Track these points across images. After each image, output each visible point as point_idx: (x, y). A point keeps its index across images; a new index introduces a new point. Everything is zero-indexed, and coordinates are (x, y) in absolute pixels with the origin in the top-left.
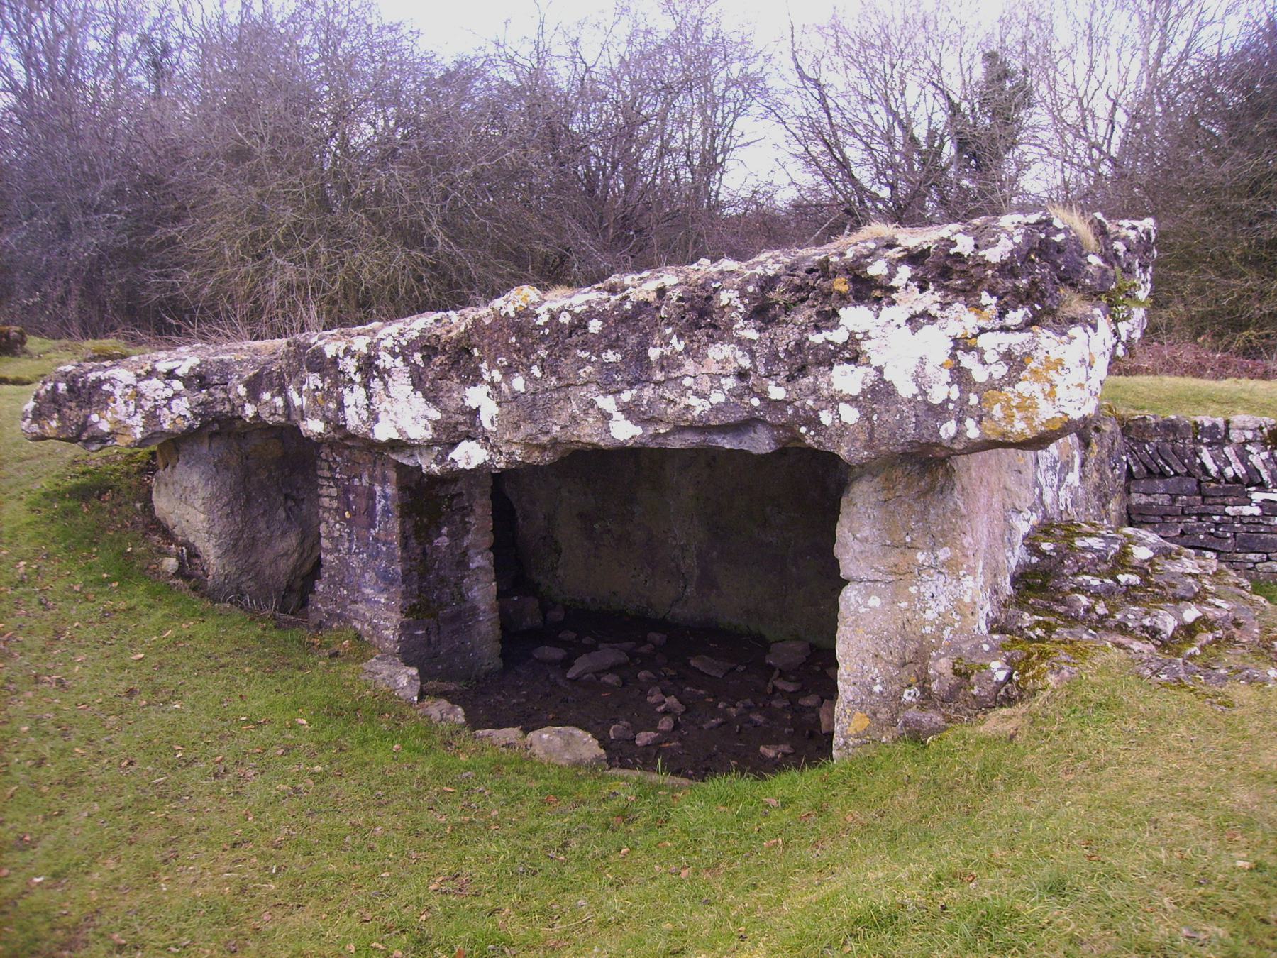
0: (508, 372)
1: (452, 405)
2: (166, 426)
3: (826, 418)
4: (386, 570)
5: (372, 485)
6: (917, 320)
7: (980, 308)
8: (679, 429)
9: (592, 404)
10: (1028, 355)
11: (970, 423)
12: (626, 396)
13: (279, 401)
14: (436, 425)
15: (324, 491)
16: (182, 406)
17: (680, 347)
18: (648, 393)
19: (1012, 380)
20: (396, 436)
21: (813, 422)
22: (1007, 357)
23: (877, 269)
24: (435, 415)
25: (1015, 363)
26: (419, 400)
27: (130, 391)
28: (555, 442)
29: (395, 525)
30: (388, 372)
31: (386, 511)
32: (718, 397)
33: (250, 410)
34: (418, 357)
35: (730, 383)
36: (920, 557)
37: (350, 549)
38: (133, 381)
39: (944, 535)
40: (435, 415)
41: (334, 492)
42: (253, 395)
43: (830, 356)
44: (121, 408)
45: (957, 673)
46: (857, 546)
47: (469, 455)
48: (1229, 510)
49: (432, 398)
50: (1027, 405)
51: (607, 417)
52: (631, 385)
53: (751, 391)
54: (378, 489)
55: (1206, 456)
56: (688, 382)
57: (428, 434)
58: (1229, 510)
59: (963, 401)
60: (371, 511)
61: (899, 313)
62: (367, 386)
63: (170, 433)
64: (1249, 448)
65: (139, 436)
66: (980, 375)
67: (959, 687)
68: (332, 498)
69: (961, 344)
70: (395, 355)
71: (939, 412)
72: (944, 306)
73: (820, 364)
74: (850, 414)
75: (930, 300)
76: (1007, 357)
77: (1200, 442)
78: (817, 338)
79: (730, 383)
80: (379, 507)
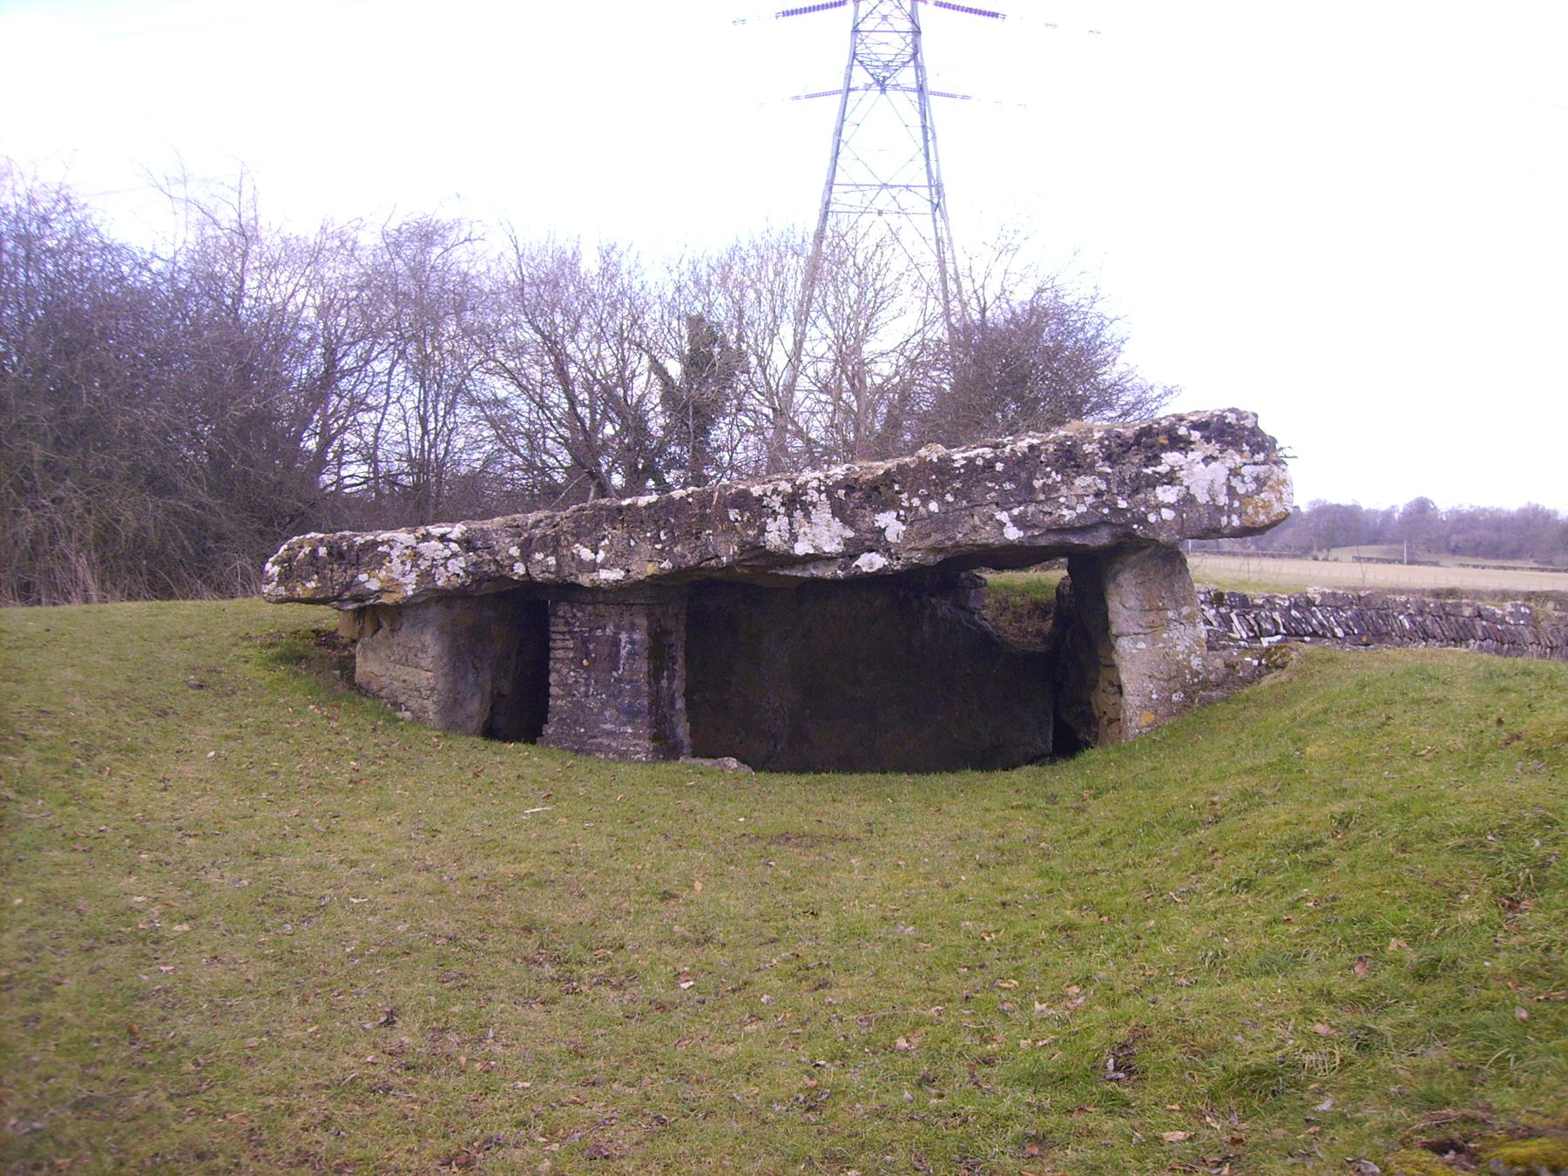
0: (925, 500)
1: (864, 526)
2: (440, 583)
3: (1152, 518)
4: (631, 705)
5: (616, 634)
6: (1207, 460)
7: (1241, 452)
8: (1049, 531)
9: (992, 517)
10: (1268, 478)
11: (1234, 517)
12: (1015, 512)
13: (552, 560)
15: (559, 644)
16: (457, 565)
17: (1059, 478)
18: (1031, 509)
19: (1258, 491)
20: (812, 551)
21: (1143, 520)
22: (1257, 479)
23: (1182, 431)
24: (850, 534)
25: (1260, 482)
26: (837, 524)
27: (408, 552)
28: (957, 545)
30: (814, 505)
31: (631, 654)
32: (1081, 509)
33: (520, 569)
34: (841, 493)
35: (1090, 500)
36: (1170, 614)
37: (586, 693)
38: (413, 542)
39: (1184, 598)
40: (850, 534)
41: (571, 644)
42: (526, 557)
45: (1227, 666)
46: (1126, 613)
47: (871, 562)
49: (848, 522)
50: (1267, 506)
51: (1002, 525)
52: (1020, 504)
53: (1104, 504)
54: (624, 637)
56: (1062, 500)
57: (840, 549)
59: (1231, 505)
60: (614, 658)
61: (1196, 455)
62: (790, 516)
63: (442, 590)
65: (410, 593)
66: (1241, 490)
67: (1228, 675)
68: (566, 649)
69: (1234, 472)
70: (820, 492)
71: (1220, 510)
72: (1221, 452)
73: (1148, 486)
74: (1167, 514)
75: (1213, 448)
76: (1257, 479)
78: (1149, 471)
79: (1090, 500)
80: (623, 652)
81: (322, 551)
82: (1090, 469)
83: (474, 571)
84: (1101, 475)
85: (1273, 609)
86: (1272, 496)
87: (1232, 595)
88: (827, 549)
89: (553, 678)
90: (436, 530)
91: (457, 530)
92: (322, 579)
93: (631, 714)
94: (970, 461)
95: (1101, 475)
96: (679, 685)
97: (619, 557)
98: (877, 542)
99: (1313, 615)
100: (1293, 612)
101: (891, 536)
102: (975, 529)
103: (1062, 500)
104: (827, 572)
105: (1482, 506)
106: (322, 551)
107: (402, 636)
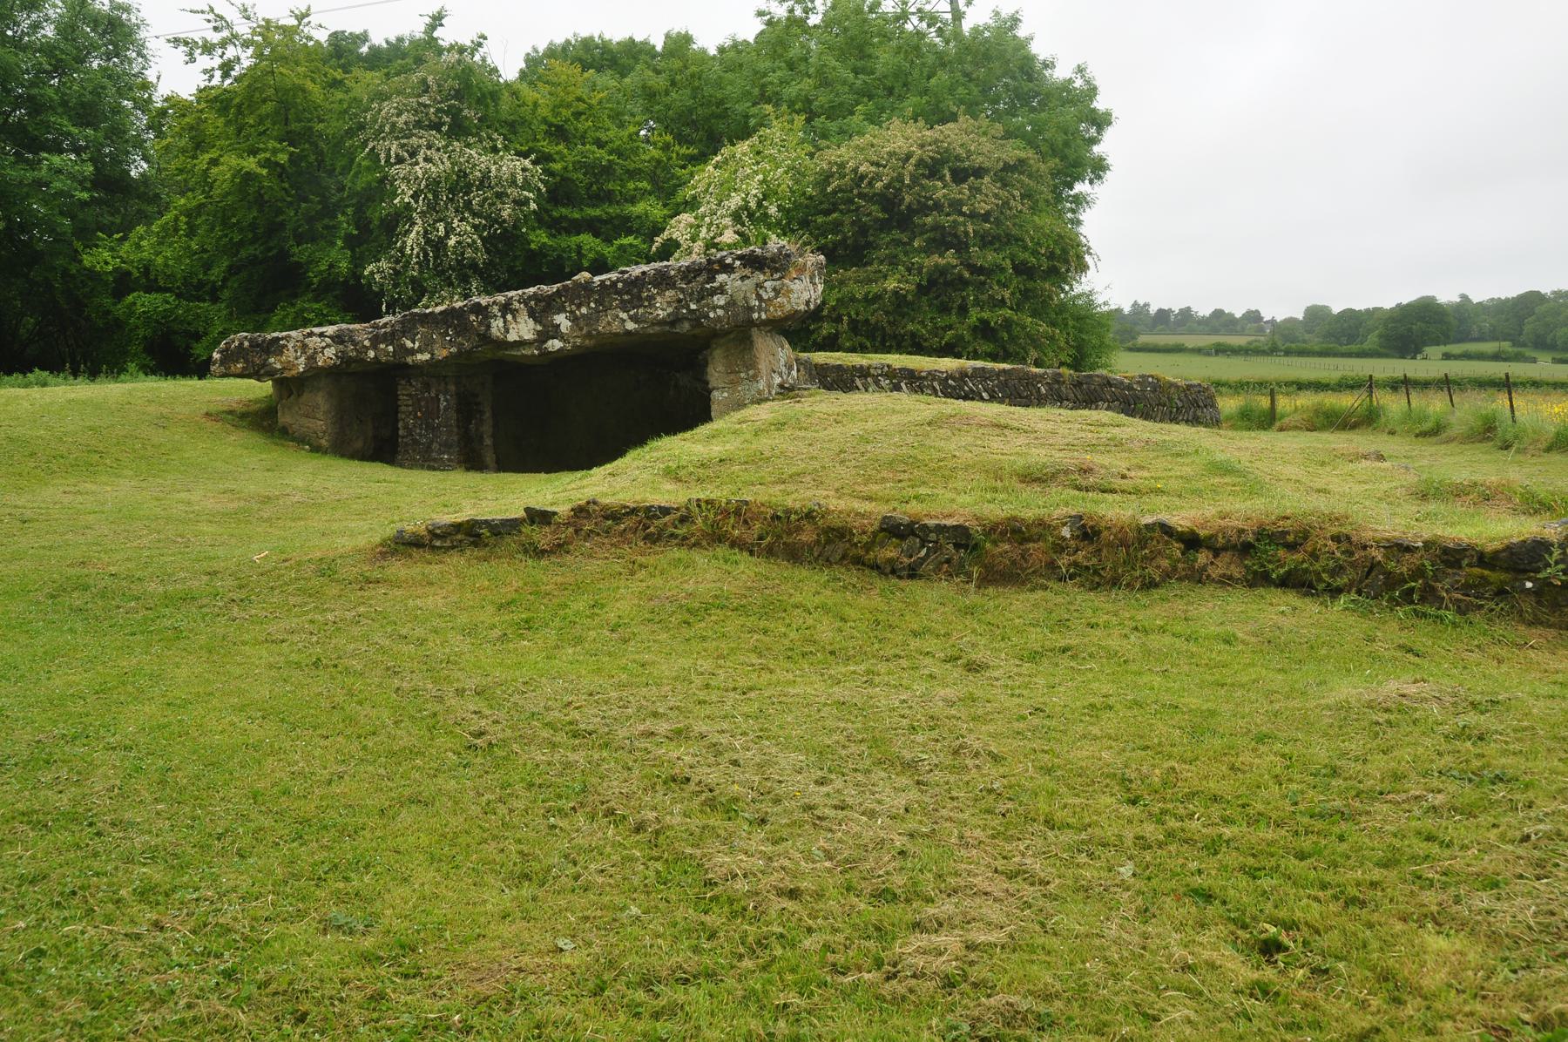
0: (579, 307)
3: (712, 315)
6: (743, 278)
13: (391, 348)
14: (539, 333)
16: (330, 352)
20: (1414, 395)
21: (707, 317)
24: (539, 328)
25: (777, 291)
29: (453, 415)
31: (446, 409)
33: (372, 354)
40: (539, 328)
42: (374, 346)
43: (713, 292)
44: (290, 354)
47: (555, 345)
50: (781, 306)
62: (504, 317)
66: (765, 297)
69: (759, 286)
74: (720, 312)
75: (747, 272)
76: (774, 289)
81: (246, 344)
82: (673, 286)
83: (342, 356)
84: (682, 290)
85: (934, 379)
89: (400, 424)
90: (317, 330)
91: (330, 330)
92: (246, 361)
93: (446, 446)
94: (603, 282)
95: (682, 290)
96: (487, 429)
97: (427, 345)
98: (554, 332)
101: (563, 329)
104: (527, 352)
105: (1360, 305)
106: (246, 344)
107: (306, 396)
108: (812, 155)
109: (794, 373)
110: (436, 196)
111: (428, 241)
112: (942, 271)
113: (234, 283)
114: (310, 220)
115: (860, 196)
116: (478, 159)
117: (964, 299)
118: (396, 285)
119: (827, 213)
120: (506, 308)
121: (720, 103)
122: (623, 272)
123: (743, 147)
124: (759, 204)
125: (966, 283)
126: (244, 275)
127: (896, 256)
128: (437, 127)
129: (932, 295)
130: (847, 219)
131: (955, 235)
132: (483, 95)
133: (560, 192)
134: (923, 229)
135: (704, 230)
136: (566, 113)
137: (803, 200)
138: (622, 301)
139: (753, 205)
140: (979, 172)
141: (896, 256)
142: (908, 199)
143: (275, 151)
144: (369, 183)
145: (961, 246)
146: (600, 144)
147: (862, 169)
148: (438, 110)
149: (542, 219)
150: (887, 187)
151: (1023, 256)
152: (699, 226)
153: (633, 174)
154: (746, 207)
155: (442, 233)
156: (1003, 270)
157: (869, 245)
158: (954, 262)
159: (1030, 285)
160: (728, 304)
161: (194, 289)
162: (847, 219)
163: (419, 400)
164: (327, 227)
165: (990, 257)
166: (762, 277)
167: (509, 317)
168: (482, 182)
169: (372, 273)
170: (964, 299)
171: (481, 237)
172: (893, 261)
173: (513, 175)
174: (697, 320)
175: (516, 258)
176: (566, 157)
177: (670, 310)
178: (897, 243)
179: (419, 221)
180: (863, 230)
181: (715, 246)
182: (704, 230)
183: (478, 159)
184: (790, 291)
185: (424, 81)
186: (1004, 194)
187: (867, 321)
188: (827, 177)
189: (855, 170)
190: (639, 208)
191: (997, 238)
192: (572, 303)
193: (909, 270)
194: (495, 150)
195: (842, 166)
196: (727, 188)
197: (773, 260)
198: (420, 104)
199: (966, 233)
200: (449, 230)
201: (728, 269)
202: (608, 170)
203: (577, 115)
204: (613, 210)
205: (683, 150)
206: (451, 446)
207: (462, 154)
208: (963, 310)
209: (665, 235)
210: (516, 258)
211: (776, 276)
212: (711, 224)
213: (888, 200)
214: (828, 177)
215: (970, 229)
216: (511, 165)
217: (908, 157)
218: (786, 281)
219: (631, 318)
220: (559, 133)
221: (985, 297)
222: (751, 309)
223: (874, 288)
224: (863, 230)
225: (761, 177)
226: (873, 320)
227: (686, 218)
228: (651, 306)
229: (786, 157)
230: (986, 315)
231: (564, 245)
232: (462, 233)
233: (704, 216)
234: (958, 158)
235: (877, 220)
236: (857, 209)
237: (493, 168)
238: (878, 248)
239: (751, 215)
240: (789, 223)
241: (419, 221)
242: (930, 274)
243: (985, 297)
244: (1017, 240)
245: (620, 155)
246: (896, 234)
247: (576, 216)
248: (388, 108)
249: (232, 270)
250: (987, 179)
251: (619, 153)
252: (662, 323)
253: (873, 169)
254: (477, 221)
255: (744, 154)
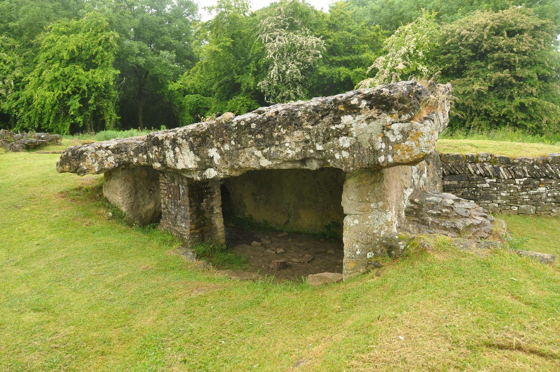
0: (223, 143)
2: (106, 166)
3: (337, 156)
6: (368, 120)
7: (392, 115)
8: (285, 162)
9: (253, 154)
12: (265, 151)
14: (199, 163)
16: (111, 159)
18: (273, 149)
19: (404, 140)
21: (333, 158)
24: (198, 159)
25: (405, 134)
27: (93, 155)
31: (183, 195)
33: (135, 160)
34: (191, 139)
36: (372, 205)
42: (136, 155)
43: (338, 134)
47: (211, 173)
48: (478, 185)
52: (267, 147)
55: (470, 167)
56: (287, 145)
58: (478, 185)
62: (173, 150)
64: (485, 164)
66: (392, 139)
69: (386, 128)
74: (345, 154)
75: (373, 113)
76: (402, 132)
77: (468, 162)
78: (333, 128)
79: (302, 145)
82: (299, 126)
84: (309, 131)
85: (524, 165)
86: (413, 143)
87: (500, 158)
88: (190, 167)
92: (70, 164)
95: (309, 131)
99: (546, 167)
100: (535, 166)
102: (247, 159)
103: (287, 145)
106: (70, 154)
108: (438, 29)
109: (425, 175)
110: (282, 54)
111: (280, 72)
112: (501, 80)
113: (219, 90)
114: (241, 66)
115: (462, 45)
116: (299, 39)
117: (512, 93)
118: (269, 90)
119: (445, 54)
120: (174, 142)
121: (401, 13)
122: (260, 113)
123: (409, 26)
124: (415, 51)
125: (511, 85)
126: (222, 86)
127: (478, 73)
128: (284, 27)
129: (495, 91)
130: (455, 57)
131: (509, 62)
132: (302, 14)
133: (333, 50)
134: (493, 60)
135: (389, 63)
136: (336, 19)
137: (434, 48)
138: (256, 140)
139: (412, 52)
140: (521, 31)
141: (478, 73)
142: (485, 46)
143: (226, 42)
144: (258, 51)
145: (511, 67)
146: (349, 31)
147: (462, 33)
148: (285, 21)
149: (325, 61)
150: (475, 41)
151: (543, 71)
152: (387, 62)
153: (364, 42)
154: (409, 53)
155: (284, 69)
156: (531, 78)
157: (465, 68)
158: (509, 75)
159: (546, 85)
160: (353, 146)
161: (208, 93)
162: (455, 57)
163: (169, 187)
164: (247, 69)
165: (526, 72)
166: (389, 119)
167: (177, 149)
168: (300, 48)
169: (260, 85)
170: (512, 93)
171: (300, 70)
172: (477, 76)
173: (313, 44)
174: (324, 160)
175: (314, 78)
176: (335, 36)
177: (298, 150)
178: (480, 67)
179: (276, 65)
180: (462, 61)
181: (395, 71)
182: (389, 63)
183: (299, 39)
184: (419, 134)
185: (280, 10)
186: (534, 41)
187: (463, 104)
188: (445, 38)
189: (459, 34)
190: (364, 56)
191: (530, 63)
192: (217, 141)
193: (485, 80)
194: (307, 35)
195: (453, 32)
196: (401, 44)
197: (401, 100)
198: (278, 19)
199: (515, 61)
200: (287, 68)
201: (353, 110)
202: (353, 40)
203: (342, 19)
204: (354, 57)
205: (385, 32)
206: (186, 219)
207: (293, 37)
208: (511, 98)
209: (372, 66)
210: (314, 78)
211: (405, 117)
212: (392, 61)
213: (475, 48)
214: (446, 37)
215: (517, 59)
216: (312, 40)
217: (485, 26)
218: (415, 123)
219: (265, 155)
220: (333, 26)
221: (522, 92)
222: (376, 153)
223: (468, 89)
224: (462, 61)
225: (415, 39)
226: (466, 103)
227: (382, 58)
228: (281, 145)
229: (427, 31)
230: (523, 100)
231: (333, 72)
232: (293, 69)
233: (389, 57)
234: (510, 25)
235: (470, 56)
236: (460, 51)
237: (305, 42)
238: (469, 69)
239: (410, 56)
240: (428, 60)
241: (276, 65)
242: (495, 81)
243: (522, 92)
244: (539, 63)
245: (358, 35)
246: (478, 63)
247: (339, 60)
248: (266, 21)
249: (220, 85)
250: (525, 34)
251: (358, 34)
252: (292, 161)
253: (468, 32)
254: (299, 63)
255: (409, 29)
